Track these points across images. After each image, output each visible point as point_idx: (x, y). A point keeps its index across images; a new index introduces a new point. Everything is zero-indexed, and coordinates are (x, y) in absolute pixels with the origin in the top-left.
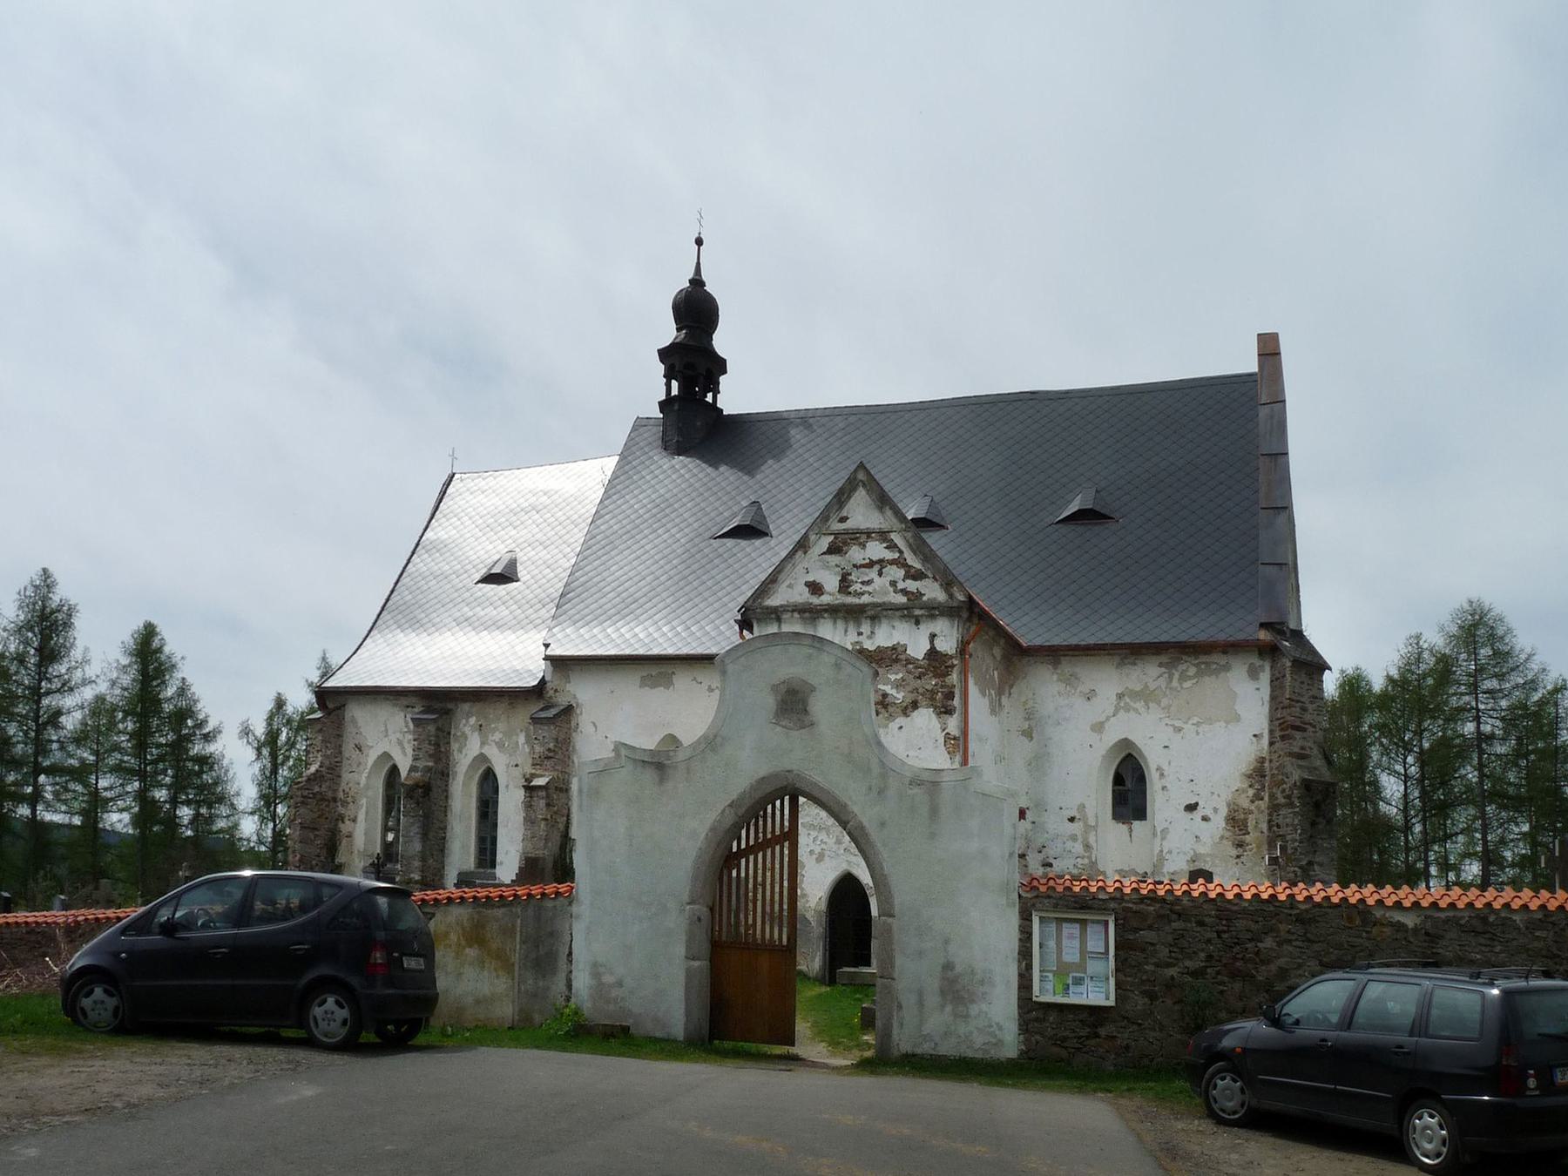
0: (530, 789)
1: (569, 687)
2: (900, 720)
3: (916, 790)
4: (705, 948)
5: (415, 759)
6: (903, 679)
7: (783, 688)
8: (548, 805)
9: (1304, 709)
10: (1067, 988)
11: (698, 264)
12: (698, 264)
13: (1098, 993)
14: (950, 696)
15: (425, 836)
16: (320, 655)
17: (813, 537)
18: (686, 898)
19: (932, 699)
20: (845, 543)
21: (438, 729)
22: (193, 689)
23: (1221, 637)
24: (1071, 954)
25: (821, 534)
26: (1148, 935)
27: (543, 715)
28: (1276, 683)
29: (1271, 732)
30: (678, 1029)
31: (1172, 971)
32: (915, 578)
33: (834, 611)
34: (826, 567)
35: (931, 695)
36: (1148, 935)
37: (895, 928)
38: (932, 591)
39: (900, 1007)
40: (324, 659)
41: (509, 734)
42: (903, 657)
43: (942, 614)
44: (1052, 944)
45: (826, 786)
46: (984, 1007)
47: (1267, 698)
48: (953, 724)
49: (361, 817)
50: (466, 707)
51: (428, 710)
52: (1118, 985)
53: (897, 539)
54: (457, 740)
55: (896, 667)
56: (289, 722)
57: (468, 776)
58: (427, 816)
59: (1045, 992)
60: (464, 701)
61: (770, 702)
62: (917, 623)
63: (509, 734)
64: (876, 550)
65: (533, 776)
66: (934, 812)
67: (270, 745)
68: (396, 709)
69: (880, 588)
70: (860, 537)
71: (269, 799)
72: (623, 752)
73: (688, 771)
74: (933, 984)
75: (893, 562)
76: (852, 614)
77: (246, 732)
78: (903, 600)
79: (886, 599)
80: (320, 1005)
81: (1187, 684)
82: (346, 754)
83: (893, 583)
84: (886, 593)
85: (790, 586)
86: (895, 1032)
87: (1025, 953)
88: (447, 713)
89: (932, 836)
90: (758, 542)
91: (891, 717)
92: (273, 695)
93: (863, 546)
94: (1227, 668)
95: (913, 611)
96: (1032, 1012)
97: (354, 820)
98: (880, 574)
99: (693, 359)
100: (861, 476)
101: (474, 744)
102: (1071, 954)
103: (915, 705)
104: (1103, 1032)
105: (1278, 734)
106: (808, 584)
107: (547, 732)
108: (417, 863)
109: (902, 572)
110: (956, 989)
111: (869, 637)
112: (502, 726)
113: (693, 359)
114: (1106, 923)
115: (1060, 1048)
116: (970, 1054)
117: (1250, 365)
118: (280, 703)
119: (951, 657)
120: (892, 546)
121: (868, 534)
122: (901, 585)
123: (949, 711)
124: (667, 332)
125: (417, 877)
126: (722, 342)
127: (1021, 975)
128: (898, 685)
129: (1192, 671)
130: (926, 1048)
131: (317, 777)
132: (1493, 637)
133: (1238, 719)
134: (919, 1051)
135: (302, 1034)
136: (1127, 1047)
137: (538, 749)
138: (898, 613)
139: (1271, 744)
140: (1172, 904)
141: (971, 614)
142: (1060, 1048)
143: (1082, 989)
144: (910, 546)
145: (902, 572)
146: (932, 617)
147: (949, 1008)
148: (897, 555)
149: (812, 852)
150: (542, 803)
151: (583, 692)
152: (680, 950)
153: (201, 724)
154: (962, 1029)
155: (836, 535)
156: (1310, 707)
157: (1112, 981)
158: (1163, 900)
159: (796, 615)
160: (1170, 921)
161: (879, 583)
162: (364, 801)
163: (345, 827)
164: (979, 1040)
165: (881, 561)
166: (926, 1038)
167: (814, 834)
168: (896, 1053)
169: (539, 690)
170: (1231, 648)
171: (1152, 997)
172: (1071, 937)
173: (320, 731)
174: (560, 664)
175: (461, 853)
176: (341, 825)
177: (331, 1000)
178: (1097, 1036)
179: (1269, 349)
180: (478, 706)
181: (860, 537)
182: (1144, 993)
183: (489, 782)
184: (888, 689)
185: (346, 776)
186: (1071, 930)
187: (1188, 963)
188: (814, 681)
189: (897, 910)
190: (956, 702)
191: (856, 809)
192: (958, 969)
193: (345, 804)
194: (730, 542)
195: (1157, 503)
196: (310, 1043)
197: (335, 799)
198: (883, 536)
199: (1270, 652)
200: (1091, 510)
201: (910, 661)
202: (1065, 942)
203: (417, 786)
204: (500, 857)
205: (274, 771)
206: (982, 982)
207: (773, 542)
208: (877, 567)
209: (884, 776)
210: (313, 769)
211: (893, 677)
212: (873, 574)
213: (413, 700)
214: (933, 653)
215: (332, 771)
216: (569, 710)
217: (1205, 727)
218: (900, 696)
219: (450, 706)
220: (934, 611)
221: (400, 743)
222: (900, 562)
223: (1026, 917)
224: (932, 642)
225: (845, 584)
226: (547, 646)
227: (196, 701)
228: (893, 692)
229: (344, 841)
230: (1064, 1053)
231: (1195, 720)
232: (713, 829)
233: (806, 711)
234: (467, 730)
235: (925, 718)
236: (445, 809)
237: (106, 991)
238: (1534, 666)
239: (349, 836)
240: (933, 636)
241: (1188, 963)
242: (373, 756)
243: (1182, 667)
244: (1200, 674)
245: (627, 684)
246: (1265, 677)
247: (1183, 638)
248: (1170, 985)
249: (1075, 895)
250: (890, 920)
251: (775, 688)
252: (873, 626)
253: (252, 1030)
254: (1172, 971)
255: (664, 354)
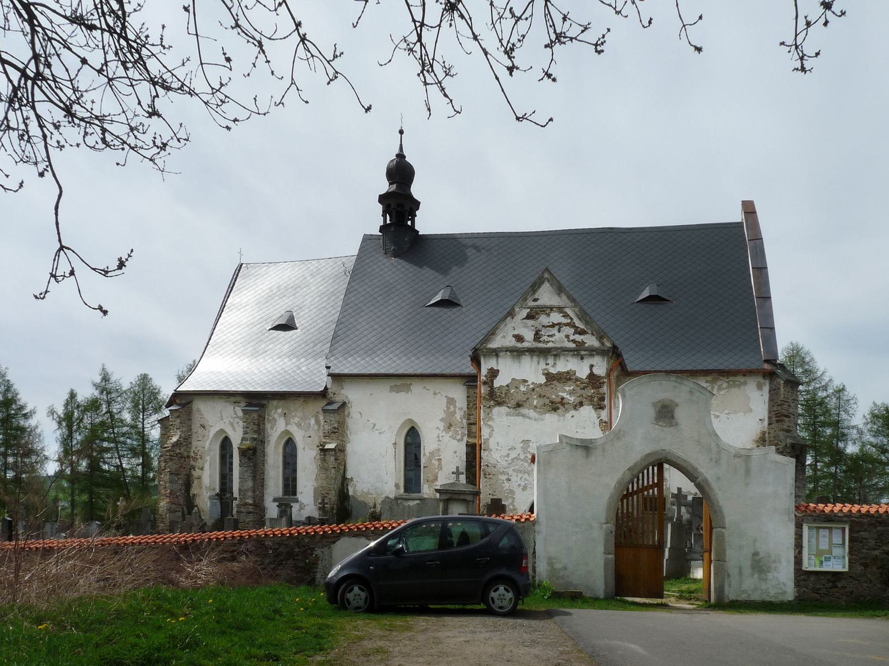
0: (324, 451)
1: (343, 392)
2: (573, 412)
3: (737, 460)
4: (612, 548)
5: (245, 433)
6: (574, 390)
7: (659, 405)
8: (336, 459)
9: (789, 406)
10: (821, 562)
11: (401, 145)
12: (401, 145)
13: (838, 564)
14: (602, 399)
15: (254, 478)
16: (100, 367)
17: (517, 310)
18: (604, 521)
19: (591, 401)
20: (537, 313)
21: (259, 416)
22: (15, 387)
23: (743, 367)
24: (824, 545)
25: (521, 307)
26: (864, 534)
27: (330, 407)
28: (773, 393)
29: (770, 418)
30: (601, 594)
31: (876, 553)
32: (580, 334)
33: (531, 351)
34: (526, 326)
35: (591, 399)
36: (864, 534)
37: (726, 535)
38: (591, 341)
39: (729, 576)
40: (104, 369)
41: (304, 418)
42: (574, 377)
43: (598, 354)
44: (814, 540)
45: (684, 457)
46: (776, 575)
47: (767, 400)
48: (604, 414)
49: (207, 466)
50: (275, 403)
51: (249, 405)
52: (850, 562)
53: (569, 311)
54: (269, 421)
55: (570, 383)
56: (78, 406)
57: (277, 443)
58: (255, 466)
59: (810, 564)
60: (274, 399)
61: (651, 412)
62: (582, 358)
63: (304, 418)
64: (556, 317)
65: (325, 443)
66: (748, 471)
67: (68, 421)
68: (228, 404)
69: (559, 339)
70: (547, 310)
71: (67, 450)
72: (564, 440)
73: (603, 450)
74: (747, 564)
75: (566, 325)
76: (543, 353)
77: (52, 412)
78: (574, 346)
79: (563, 345)
80: (495, 591)
81: (722, 392)
82: (194, 430)
83: (567, 336)
84: (563, 342)
85: (504, 337)
86: (726, 588)
87: (799, 546)
88: (190, 402)
89: (747, 484)
90: (455, 310)
91: (567, 411)
92: (68, 391)
93: (548, 315)
94: (745, 383)
95: (580, 351)
96: (802, 576)
97: (202, 469)
98: (559, 331)
99: (399, 203)
100: (546, 275)
101: (278, 425)
102: (824, 545)
103: (581, 404)
104: (839, 585)
105: (774, 419)
106: (515, 336)
107: (333, 418)
108: (250, 494)
109: (573, 330)
110: (760, 565)
111: (553, 366)
112: (299, 414)
113: (399, 203)
114: (843, 529)
115: (817, 594)
116: (768, 599)
117: (736, 216)
118: (73, 395)
119: (603, 378)
120: (566, 316)
121: (551, 308)
122: (572, 337)
123: (602, 408)
124: (384, 186)
125: (250, 501)
126: (417, 190)
127: (796, 557)
128: (571, 393)
129: (725, 385)
130: (743, 597)
131: (177, 444)
132: (803, 362)
133: (751, 411)
134: (739, 599)
135: (482, 606)
136: (852, 593)
137: (326, 427)
138: (571, 353)
139: (769, 424)
140: (878, 517)
141: (614, 354)
142: (817, 594)
143: (830, 563)
144: (577, 316)
145: (573, 330)
146: (592, 355)
147: (756, 576)
148: (569, 321)
149: (519, 485)
150: (332, 458)
151: (352, 394)
152: (601, 549)
153: (22, 408)
154: (764, 586)
155: (531, 308)
156: (792, 405)
157: (847, 559)
158: (872, 516)
159: (508, 353)
160: (876, 527)
161: (559, 336)
162: (208, 458)
163: (196, 473)
164: (773, 592)
165: (559, 324)
166: (744, 592)
167: (520, 475)
168: (727, 601)
169: (324, 394)
170: (748, 373)
171: (866, 566)
172: (824, 536)
173: (179, 417)
174: (337, 378)
175: (274, 486)
176: (193, 472)
177: (502, 588)
178: (836, 587)
179: (749, 209)
180: (282, 403)
181: (547, 310)
182: (861, 564)
183: (226, 444)
184: (564, 395)
185: (195, 443)
186: (824, 533)
187: (885, 548)
188: (677, 400)
189: (727, 526)
190: (606, 402)
191: (702, 470)
192: (761, 555)
193: (195, 459)
194: (437, 309)
195: (685, 295)
196: (489, 612)
197: (188, 457)
198: (560, 310)
199: (770, 375)
200: (657, 296)
201: (577, 380)
202: (821, 539)
203: (249, 449)
204: (300, 488)
205: (70, 435)
206: (774, 561)
207: (464, 309)
208: (557, 327)
209: (719, 452)
210: (174, 439)
211: (567, 389)
212: (555, 331)
213: (239, 399)
214: (592, 376)
215: (186, 441)
216: (344, 405)
217: (733, 416)
218: (572, 399)
219: (264, 402)
220: (592, 352)
221: (231, 424)
222: (571, 325)
223: (799, 526)
224: (591, 370)
225: (537, 337)
226: (328, 368)
227: (17, 394)
228: (568, 397)
229: (196, 482)
230: (818, 596)
231: (727, 411)
232: (619, 483)
233: (673, 417)
234: (276, 416)
235: (587, 411)
236: (264, 462)
237: (360, 588)
238: (826, 378)
239: (199, 478)
240: (592, 366)
241: (885, 548)
242: (213, 431)
243: (719, 383)
244: (729, 387)
245: (381, 391)
246: (766, 388)
247: (721, 367)
248: (875, 559)
249: (826, 515)
250: (723, 530)
251: (654, 404)
252: (555, 360)
253: (449, 606)
254: (876, 553)
255: (383, 199)
